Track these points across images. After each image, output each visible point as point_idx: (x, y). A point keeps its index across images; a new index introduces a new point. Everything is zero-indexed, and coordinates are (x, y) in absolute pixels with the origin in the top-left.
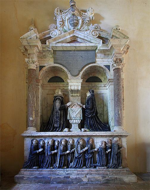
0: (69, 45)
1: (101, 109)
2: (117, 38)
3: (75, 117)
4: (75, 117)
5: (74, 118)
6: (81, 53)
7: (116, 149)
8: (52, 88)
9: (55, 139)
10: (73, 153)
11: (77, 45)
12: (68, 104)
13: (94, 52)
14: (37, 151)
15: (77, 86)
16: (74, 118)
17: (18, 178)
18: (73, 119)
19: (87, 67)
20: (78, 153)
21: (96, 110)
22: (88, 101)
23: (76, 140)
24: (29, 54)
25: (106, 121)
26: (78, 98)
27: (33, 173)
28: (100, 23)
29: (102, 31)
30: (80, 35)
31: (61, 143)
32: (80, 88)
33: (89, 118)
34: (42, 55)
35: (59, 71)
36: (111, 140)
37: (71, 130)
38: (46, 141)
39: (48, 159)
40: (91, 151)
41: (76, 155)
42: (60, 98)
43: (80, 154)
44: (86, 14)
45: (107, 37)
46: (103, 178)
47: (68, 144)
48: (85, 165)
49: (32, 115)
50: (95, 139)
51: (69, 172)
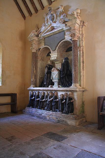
0: (52, 32)
4: (55, 78)
14: (32, 98)
15: (55, 57)
19: (60, 43)
26: (60, 65)
30: (54, 25)
39: (36, 103)
49: (32, 78)
50: (58, 92)
51: (43, 112)
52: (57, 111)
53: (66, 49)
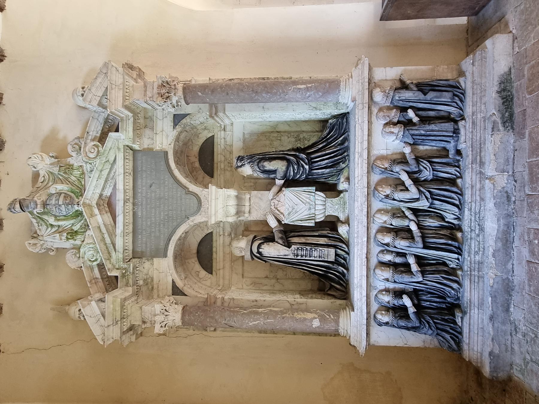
0: (120, 219)
1: (285, 138)
2: (105, 94)
3: (308, 206)
5: (310, 209)
6: (142, 189)
7: (407, 95)
8: (228, 265)
9: (374, 261)
10: (415, 211)
11: (120, 196)
12: (273, 223)
13: (139, 155)
16: (310, 209)
17: (495, 369)
18: (313, 211)
19: (177, 173)
20: (417, 200)
21: (289, 150)
22: (265, 172)
23: (377, 205)
24: (144, 322)
25: (317, 127)
27: (476, 327)
28: (65, 138)
29: (85, 132)
31: (387, 245)
32: (232, 192)
33: (311, 169)
34: (144, 289)
35: (184, 244)
36: (381, 110)
37: (342, 218)
38: (382, 285)
40: (412, 162)
41: (423, 204)
42: (256, 244)
43: (420, 192)
44: (42, 173)
45: (101, 120)
46: (499, 130)
47: (391, 225)
48: (452, 182)
49: (305, 319)
52: (458, 152)
53: (201, 173)
